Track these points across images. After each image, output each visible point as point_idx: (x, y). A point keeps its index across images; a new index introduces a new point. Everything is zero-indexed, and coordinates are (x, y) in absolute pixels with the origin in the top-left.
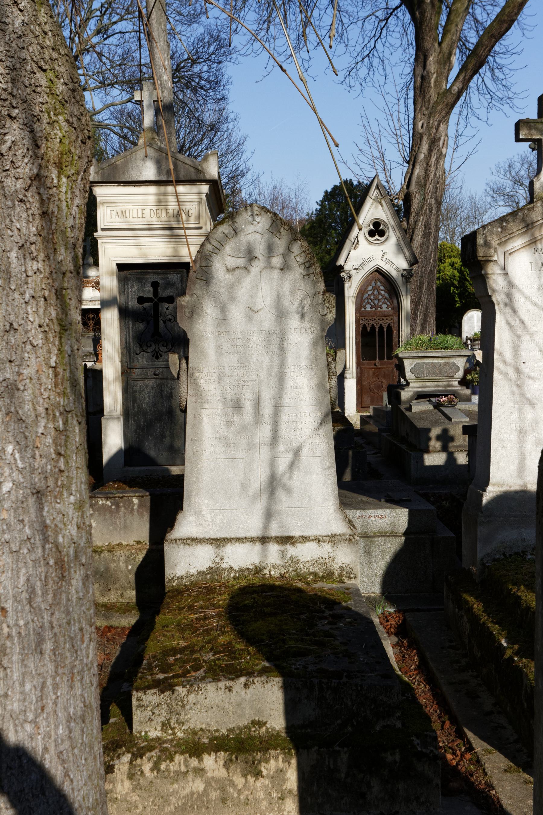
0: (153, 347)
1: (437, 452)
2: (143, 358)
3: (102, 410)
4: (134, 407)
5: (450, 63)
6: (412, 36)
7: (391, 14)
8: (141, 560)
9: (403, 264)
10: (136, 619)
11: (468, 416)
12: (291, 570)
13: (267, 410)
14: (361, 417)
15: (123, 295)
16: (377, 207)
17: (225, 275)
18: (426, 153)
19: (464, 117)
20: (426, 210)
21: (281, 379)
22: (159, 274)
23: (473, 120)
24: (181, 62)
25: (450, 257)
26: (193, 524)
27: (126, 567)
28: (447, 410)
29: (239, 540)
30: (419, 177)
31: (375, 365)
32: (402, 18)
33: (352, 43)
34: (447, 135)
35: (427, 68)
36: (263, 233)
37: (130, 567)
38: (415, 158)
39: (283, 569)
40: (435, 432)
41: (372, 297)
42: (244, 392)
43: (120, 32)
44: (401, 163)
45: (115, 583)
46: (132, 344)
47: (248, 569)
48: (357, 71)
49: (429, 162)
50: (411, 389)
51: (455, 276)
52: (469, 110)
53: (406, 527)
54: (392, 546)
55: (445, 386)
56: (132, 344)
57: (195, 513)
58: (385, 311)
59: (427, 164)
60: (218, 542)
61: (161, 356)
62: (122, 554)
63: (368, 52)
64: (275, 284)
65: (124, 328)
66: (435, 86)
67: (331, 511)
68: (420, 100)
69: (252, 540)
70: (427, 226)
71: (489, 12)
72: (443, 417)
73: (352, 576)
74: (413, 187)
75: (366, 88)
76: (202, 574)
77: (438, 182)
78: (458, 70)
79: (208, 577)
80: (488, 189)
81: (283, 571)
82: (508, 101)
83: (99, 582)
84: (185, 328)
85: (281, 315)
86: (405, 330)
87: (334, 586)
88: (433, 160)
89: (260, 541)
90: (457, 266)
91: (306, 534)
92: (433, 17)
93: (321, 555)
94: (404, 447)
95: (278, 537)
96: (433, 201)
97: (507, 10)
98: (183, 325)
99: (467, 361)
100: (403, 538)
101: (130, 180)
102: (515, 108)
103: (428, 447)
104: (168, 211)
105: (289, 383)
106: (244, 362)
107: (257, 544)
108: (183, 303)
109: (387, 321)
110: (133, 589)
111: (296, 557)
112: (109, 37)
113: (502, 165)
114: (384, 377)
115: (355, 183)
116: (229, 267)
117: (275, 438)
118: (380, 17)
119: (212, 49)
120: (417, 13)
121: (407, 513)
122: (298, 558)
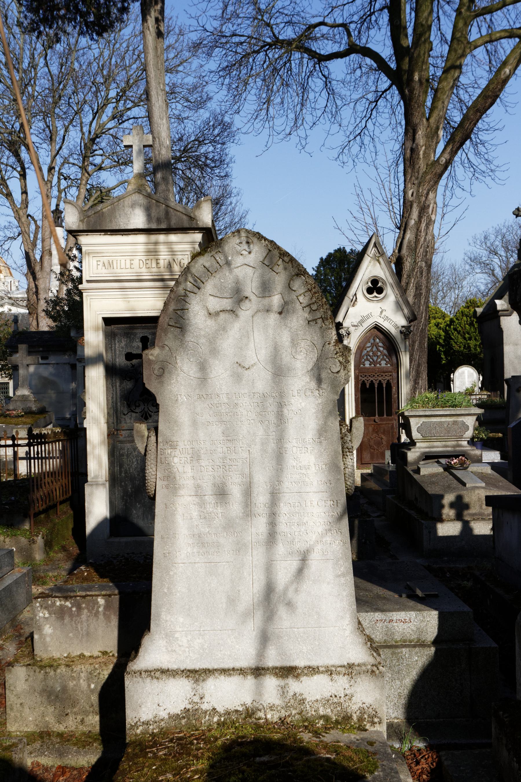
0: (142, 407)
1: (452, 520)
2: (130, 419)
3: (86, 474)
4: (121, 472)
5: (438, 136)
6: (401, 117)
7: (381, 96)
8: (106, 677)
9: (403, 322)
10: (98, 757)
11: (482, 480)
12: (294, 712)
13: (261, 499)
14: (362, 475)
15: (110, 351)
16: (374, 265)
17: (206, 321)
18: (417, 219)
19: (449, 189)
20: (417, 273)
21: (279, 457)
22: (148, 328)
23: (458, 191)
24: (188, 144)
25: (435, 318)
26: (164, 649)
27: (87, 686)
28: (459, 473)
29: (225, 671)
30: (409, 242)
31: (375, 421)
32: (390, 100)
33: (345, 123)
34: (435, 203)
35: (416, 141)
36: (255, 266)
37: (93, 686)
38: (406, 224)
39: (283, 711)
40: (449, 498)
41: (371, 354)
42: (231, 473)
43: (134, 118)
44: (393, 229)
45: (73, 706)
46: (119, 404)
47: (237, 711)
48: (350, 148)
49: (419, 227)
50: (417, 450)
51: (440, 335)
52: (454, 182)
53: (435, 634)
54: (418, 660)
55: (454, 446)
56: (119, 404)
57: (166, 635)
58: (384, 367)
59: (418, 230)
60: (197, 675)
61: (151, 416)
62: (83, 669)
63: (359, 131)
64: (271, 331)
65: (110, 386)
66: (423, 157)
67: (348, 633)
68: (410, 171)
69: (242, 672)
70: (418, 287)
71: (471, 94)
72: (455, 481)
73: (376, 720)
74: (404, 251)
75: (358, 163)
76: (176, 717)
77: (428, 246)
78: (443, 147)
79: (183, 722)
80: (466, 258)
81: (283, 714)
82: (491, 174)
83: (54, 705)
84: (153, 390)
85: (279, 372)
86: (405, 388)
87: (353, 736)
88: (423, 225)
89: (253, 673)
90: (442, 326)
91: (314, 663)
92: (421, 94)
93: (334, 692)
94: (412, 512)
95: (276, 668)
96: (424, 264)
97: (491, 87)
98: (151, 386)
99: (477, 420)
100: (433, 649)
101: (117, 228)
102: (497, 180)
103: (441, 515)
104: (159, 261)
105: (290, 462)
106: (230, 436)
107: (249, 677)
108: (151, 357)
109: (387, 378)
110: (96, 715)
111: (301, 694)
112: (124, 122)
113: (478, 236)
114: (384, 433)
115: (348, 250)
116: (212, 311)
117: (272, 537)
118: (371, 100)
119: (216, 132)
120: (407, 91)
121: (437, 616)
122: (304, 697)
